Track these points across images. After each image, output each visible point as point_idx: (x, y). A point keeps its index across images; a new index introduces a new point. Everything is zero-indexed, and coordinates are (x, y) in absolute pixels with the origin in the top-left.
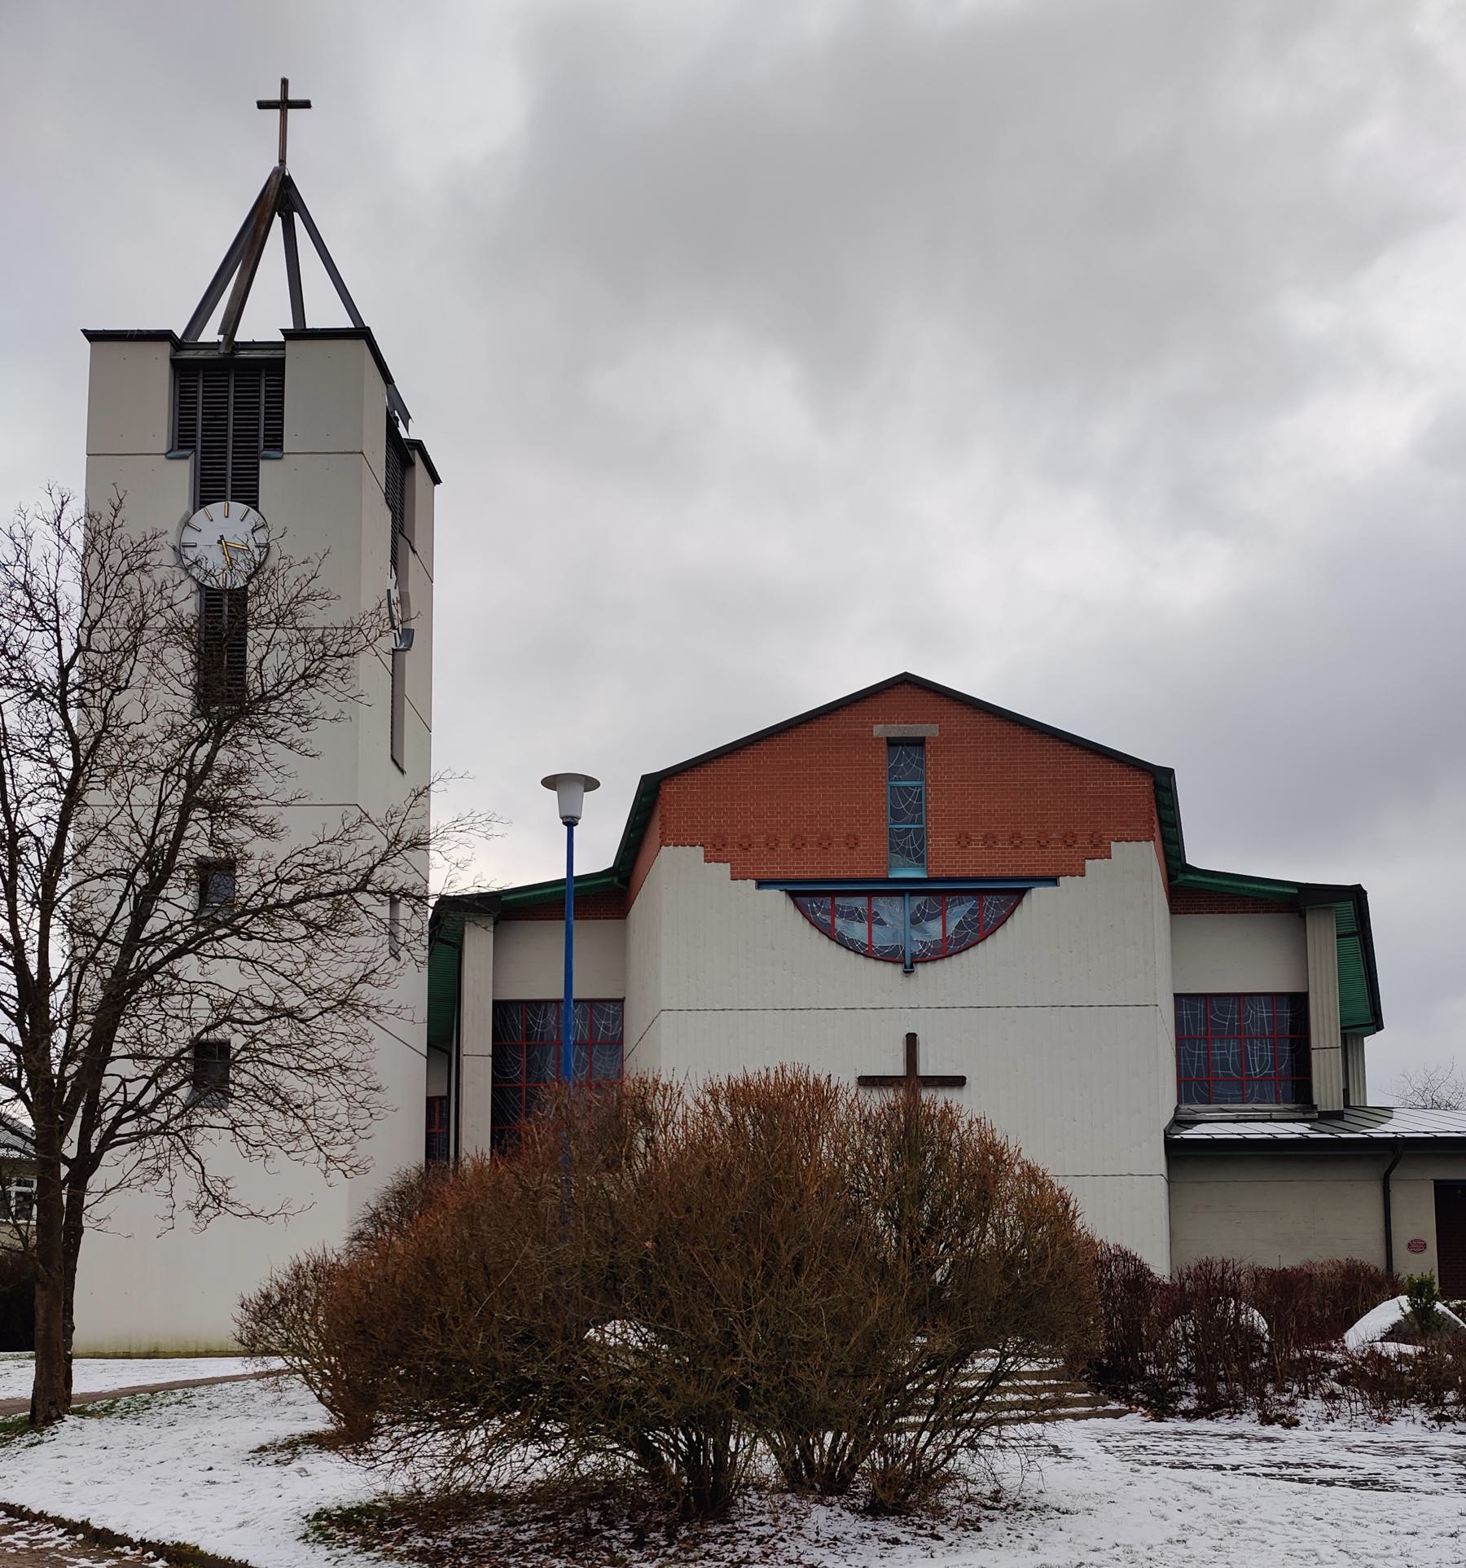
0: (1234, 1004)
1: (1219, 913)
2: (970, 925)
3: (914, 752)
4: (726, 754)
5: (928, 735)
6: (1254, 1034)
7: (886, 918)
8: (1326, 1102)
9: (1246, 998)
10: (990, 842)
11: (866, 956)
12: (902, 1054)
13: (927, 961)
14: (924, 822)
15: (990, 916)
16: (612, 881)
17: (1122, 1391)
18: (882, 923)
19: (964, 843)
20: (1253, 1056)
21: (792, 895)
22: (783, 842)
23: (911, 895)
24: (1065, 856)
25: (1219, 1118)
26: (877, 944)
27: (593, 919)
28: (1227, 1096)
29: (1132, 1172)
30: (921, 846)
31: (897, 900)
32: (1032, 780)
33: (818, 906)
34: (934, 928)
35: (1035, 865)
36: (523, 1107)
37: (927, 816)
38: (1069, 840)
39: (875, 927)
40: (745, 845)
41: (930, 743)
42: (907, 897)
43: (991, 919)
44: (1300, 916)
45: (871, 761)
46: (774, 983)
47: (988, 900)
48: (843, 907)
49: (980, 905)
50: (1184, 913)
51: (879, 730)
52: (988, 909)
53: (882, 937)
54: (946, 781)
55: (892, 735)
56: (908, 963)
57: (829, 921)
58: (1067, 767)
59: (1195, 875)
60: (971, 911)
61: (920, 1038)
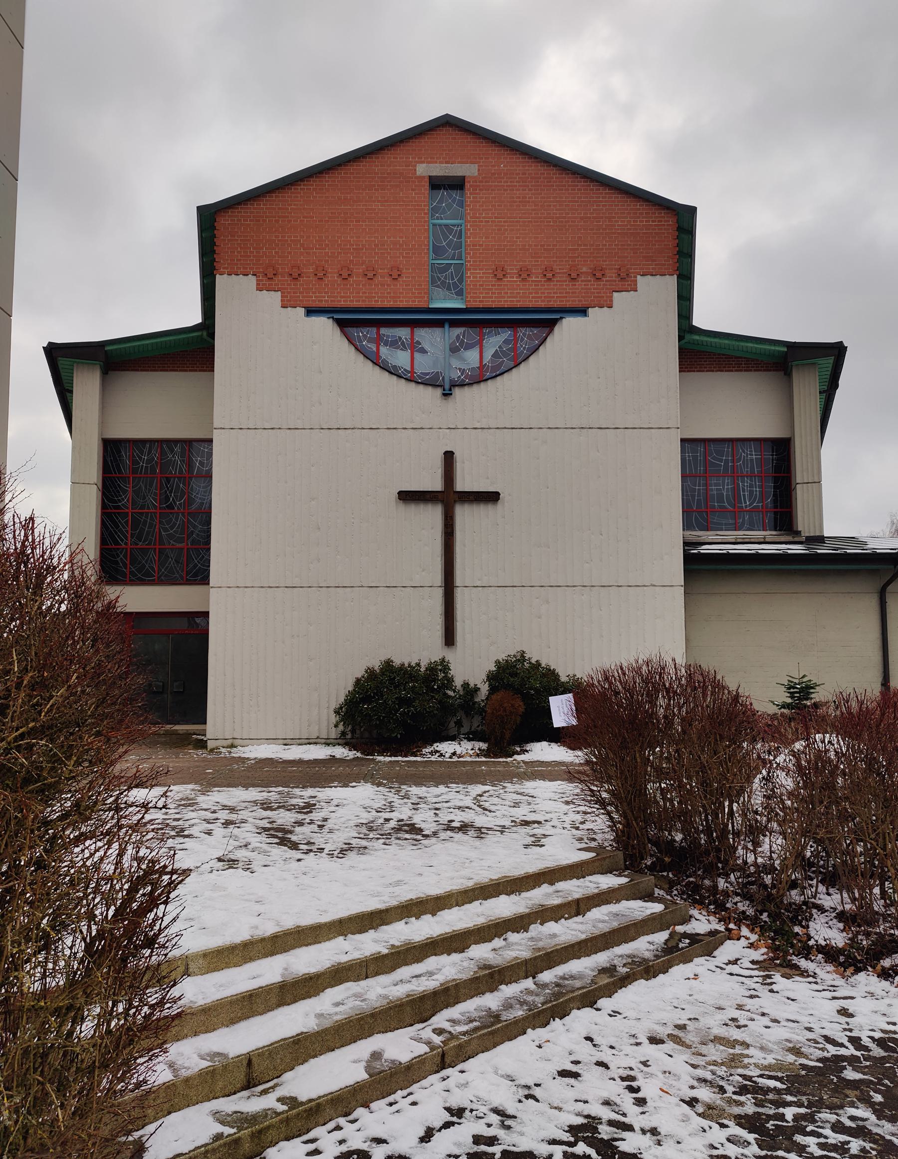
0: (728, 448)
1: (717, 371)
2: (505, 354)
3: (456, 195)
4: (278, 189)
5: (467, 174)
6: (745, 473)
7: (426, 346)
8: (809, 529)
9: (712, 446)
10: (524, 275)
11: (408, 380)
12: (440, 471)
13: (465, 385)
14: (463, 258)
15: (523, 346)
16: (202, 335)
17: (708, 890)
18: (423, 351)
19: (500, 275)
20: (744, 491)
21: (342, 324)
22: (331, 273)
23: (450, 326)
24: (594, 289)
25: (720, 541)
26: (419, 370)
27: (190, 371)
28: (721, 524)
29: (654, 583)
30: (461, 280)
31: (437, 332)
32: (565, 218)
33: (364, 335)
34: (472, 357)
35: (566, 297)
36: (129, 529)
37: (466, 250)
38: (597, 274)
39: (417, 355)
40: (295, 275)
41: (469, 182)
42: (447, 326)
43: (524, 348)
44: (785, 374)
45: (415, 197)
46: (321, 404)
47: (522, 331)
48: (388, 336)
49: (515, 335)
50: (688, 371)
51: (423, 170)
52: (522, 340)
53: (424, 364)
54: (484, 218)
55: (434, 174)
56: (447, 387)
57: (375, 349)
58: (597, 206)
59: (699, 335)
60: (506, 342)
61: (458, 455)
